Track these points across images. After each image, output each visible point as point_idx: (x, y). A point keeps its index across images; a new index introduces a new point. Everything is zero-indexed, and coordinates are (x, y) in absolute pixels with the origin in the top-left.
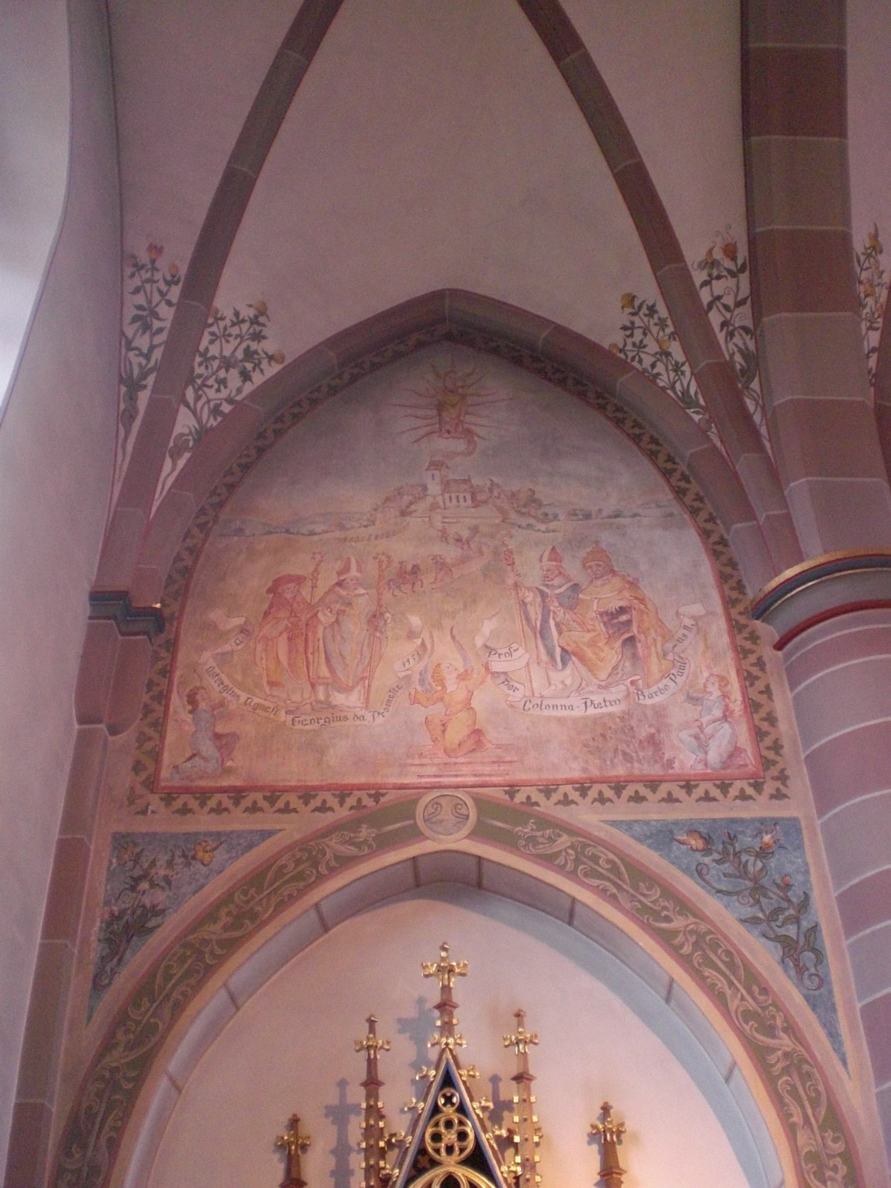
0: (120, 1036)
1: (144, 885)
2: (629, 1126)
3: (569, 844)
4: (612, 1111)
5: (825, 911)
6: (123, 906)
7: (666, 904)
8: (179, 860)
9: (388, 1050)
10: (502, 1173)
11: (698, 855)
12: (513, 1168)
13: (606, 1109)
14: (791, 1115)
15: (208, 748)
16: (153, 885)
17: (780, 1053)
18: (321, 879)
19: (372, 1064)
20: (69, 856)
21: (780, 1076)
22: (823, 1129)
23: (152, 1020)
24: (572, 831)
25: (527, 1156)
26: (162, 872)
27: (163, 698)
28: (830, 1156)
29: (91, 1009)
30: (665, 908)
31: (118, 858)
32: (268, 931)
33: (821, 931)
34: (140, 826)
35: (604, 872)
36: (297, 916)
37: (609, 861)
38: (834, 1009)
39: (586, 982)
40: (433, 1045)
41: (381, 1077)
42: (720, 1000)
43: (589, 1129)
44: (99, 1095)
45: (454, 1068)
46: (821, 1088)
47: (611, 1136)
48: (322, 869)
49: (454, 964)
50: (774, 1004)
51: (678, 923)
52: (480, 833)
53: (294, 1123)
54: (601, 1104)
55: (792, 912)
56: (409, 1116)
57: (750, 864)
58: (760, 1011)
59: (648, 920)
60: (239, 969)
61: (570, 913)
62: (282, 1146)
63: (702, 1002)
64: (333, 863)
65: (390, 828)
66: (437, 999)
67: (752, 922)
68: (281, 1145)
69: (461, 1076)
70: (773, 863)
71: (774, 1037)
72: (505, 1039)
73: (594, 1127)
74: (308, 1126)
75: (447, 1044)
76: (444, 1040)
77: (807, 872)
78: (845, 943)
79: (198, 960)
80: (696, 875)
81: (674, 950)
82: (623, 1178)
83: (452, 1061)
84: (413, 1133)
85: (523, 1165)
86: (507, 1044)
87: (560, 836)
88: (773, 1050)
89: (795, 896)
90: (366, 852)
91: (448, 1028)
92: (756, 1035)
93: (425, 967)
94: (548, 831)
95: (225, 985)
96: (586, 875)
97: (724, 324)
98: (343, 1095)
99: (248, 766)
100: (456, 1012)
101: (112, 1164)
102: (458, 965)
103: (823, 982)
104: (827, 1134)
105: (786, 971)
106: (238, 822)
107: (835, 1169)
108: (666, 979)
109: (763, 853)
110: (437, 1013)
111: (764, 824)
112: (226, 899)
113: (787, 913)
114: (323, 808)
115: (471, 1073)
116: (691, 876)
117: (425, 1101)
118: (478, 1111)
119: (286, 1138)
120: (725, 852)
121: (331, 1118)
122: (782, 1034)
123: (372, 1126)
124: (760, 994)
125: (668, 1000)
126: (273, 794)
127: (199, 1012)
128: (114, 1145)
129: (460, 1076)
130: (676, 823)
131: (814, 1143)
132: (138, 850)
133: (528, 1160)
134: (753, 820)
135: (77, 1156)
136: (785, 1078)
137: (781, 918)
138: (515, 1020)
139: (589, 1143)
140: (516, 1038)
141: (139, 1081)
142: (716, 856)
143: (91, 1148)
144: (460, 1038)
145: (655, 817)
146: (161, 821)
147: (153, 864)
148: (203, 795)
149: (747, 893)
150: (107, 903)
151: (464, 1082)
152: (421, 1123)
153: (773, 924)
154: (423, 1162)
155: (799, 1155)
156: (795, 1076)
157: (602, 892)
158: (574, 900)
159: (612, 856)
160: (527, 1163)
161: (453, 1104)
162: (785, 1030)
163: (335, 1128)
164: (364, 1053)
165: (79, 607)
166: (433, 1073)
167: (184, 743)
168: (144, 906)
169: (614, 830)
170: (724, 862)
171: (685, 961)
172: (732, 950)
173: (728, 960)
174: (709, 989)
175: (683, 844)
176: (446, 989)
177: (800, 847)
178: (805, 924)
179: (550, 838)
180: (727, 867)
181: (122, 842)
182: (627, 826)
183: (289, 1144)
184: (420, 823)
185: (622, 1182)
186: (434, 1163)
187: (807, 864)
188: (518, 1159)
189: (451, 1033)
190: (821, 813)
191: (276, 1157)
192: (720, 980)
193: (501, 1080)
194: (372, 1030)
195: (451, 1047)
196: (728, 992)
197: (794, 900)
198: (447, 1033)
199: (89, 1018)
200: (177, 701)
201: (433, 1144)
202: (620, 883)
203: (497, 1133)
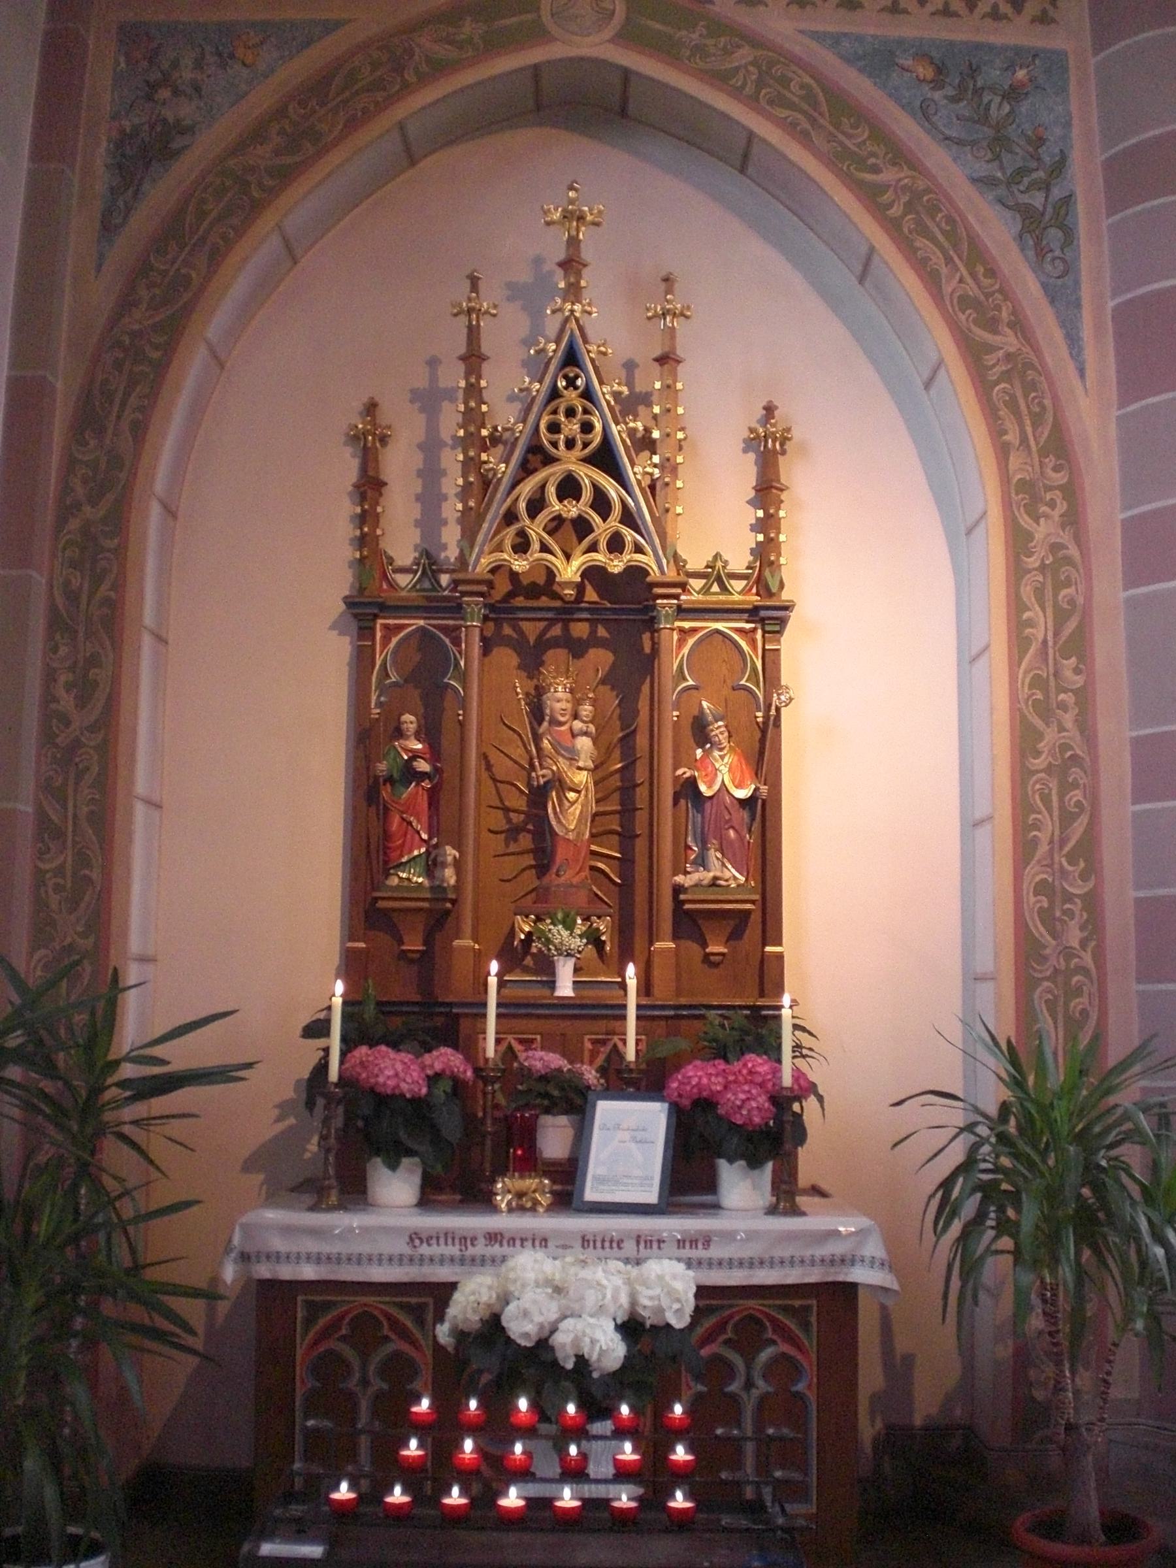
0: (143, 293)
1: (164, 94)
2: (796, 433)
3: (750, 59)
4: (776, 413)
5: (1084, 179)
6: (136, 121)
7: (875, 149)
8: (211, 59)
9: (494, 315)
10: (635, 474)
11: (926, 88)
12: (649, 470)
13: (769, 410)
14: (1005, 432)
16: (176, 92)
17: (1001, 353)
18: (407, 89)
19: (473, 333)
21: (997, 383)
22: (1043, 453)
23: (183, 271)
24: (755, 41)
25: (667, 455)
26: (187, 75)
28: (1049, 489)
29: (102, 256)
30: (873, 155)
31: (127, 55)
32: (335, 158)
33: (1075, 203)
35: (796, 99)
36: (376, 138)
37: (802, 86)
38: (1078, 305)
39: (756, 248)
40: (554, 312)
41: (485, 348)
42: (932, 280)
43: (746, 434)
44: (118, 365)
45: (580, 341)
46: (1047, 402)
47: (774, 442)
48: (410, 76)
49: (586, 209)
50: (1001, 291)
51: (888, 175)
52: (628, 36)
53: (371, 408)
54: (764, 403)
55: (1041, 174)
56: (518, 406)
57: (993, 106)
58: (982, 298)
59: (848, 166)
60: (298, 206)
61: (743, 156)
62: (354, 437)
63: (910, 280)
64: (424, 68)
65: (507, 22)
66: (561, 255)
67: (985, 183)
68: (354, 435)
69: (589, 352)
70: (1024, 107)
71: (995, 332)
72: (648, 310)
73: (751, 430)
74: (386, 415)
75: (572, 311)
76: (568, 306)
77: (1068, 125)
78: (1106, 223)
79: (243, 192)
80: (920, 114)
81: (878, 210)
82: (784, 496)
83: (577, 333)
84: (524, 421)
85: (660, 466)
86: (650, 314)
87: (739, 47)
88: (991, 349)
89: (1048, 155)
90: (470, 54)
91: (574, 292)
92: (973, 327)
93: (546, 212)
94: (723, 39)
95: (279, 226)
96: (771, 102)
98: (434, 379)
100: (586, 272)
101: (137, 455)
102: (591, 210)
103: (1069, 269)
104: (1047, 460)
105: (1022, 250)
107: (1052, 504)
108: (864, 249)
109: (1014, 94)
110: (560, 272)
111: (1017, 57)
112: (280, 112)
113: (1034, 175)
115: (602, 349)
116: (913, 115)
117: (540, 382)
118: (607, 397)
119: (360, 426)
120: (961, 88)
121: (418, 405)
122: (1007, 330)
123: (472, 409)
124: (985, 276)
125: (861, 280)
127: (245, 260)
128: (139, 431)
129: (588, 354)
130: (900, 42)
131: (1030, 469)
132: (154, 45)
133: (668, 460)
134: (1005, 48)
135: (92, 443)
136: (1003, 385)
137: (1026, 181)
138: (663, 286)
139: (745, 451)
140: (662, 309)
141: (169, 350)
142: (950, 91)
143: (110, 431)
144: (589, 304)
145: (872, 31)
147: (175, 65)
149: (985, 144)
150: (115, 117)
151: (592, 361)
152: (535, 409)
153: (1014, 188)
154: (537, 456)
155: (1008, 482)
156: (1017, 384)
157: (790, 128)
158: (751, 136)
159: (808, 80)
160: (667, 464)
161: (576, 388)
162: (1011, 325)
163: (422, 418)
164: (463, 320)
166: (553, 346)
168: (165, 120)
169: (814, 45)
170: (960, 100)
171: (892, 227)
172: (958, 219)
173: (948, 228)
174: (921, 266)
175: (907, 71)
176: (573, 242)
177: (1063, 90)
178: (1057, 193)
179: (724, 49)
180: (963, 108)
182: (835, 41)
183: (365, 434)
184: (546, 18)
185: (782, 501)
186: (549, 460)
187: (1069, 114)
188: (656, 459)
189: (577, 299)
190: (1096, 52)
191: (348, 451)
192: (934, 253)
193: (637, 366)
194: (474, 287)
195: (577, 315)
196: (944, 271)
197: (1047, 159)
198: (572, 298)
199: (99, 269)
201: (548, 435)
202: (816, 115)
203: (631, 425)
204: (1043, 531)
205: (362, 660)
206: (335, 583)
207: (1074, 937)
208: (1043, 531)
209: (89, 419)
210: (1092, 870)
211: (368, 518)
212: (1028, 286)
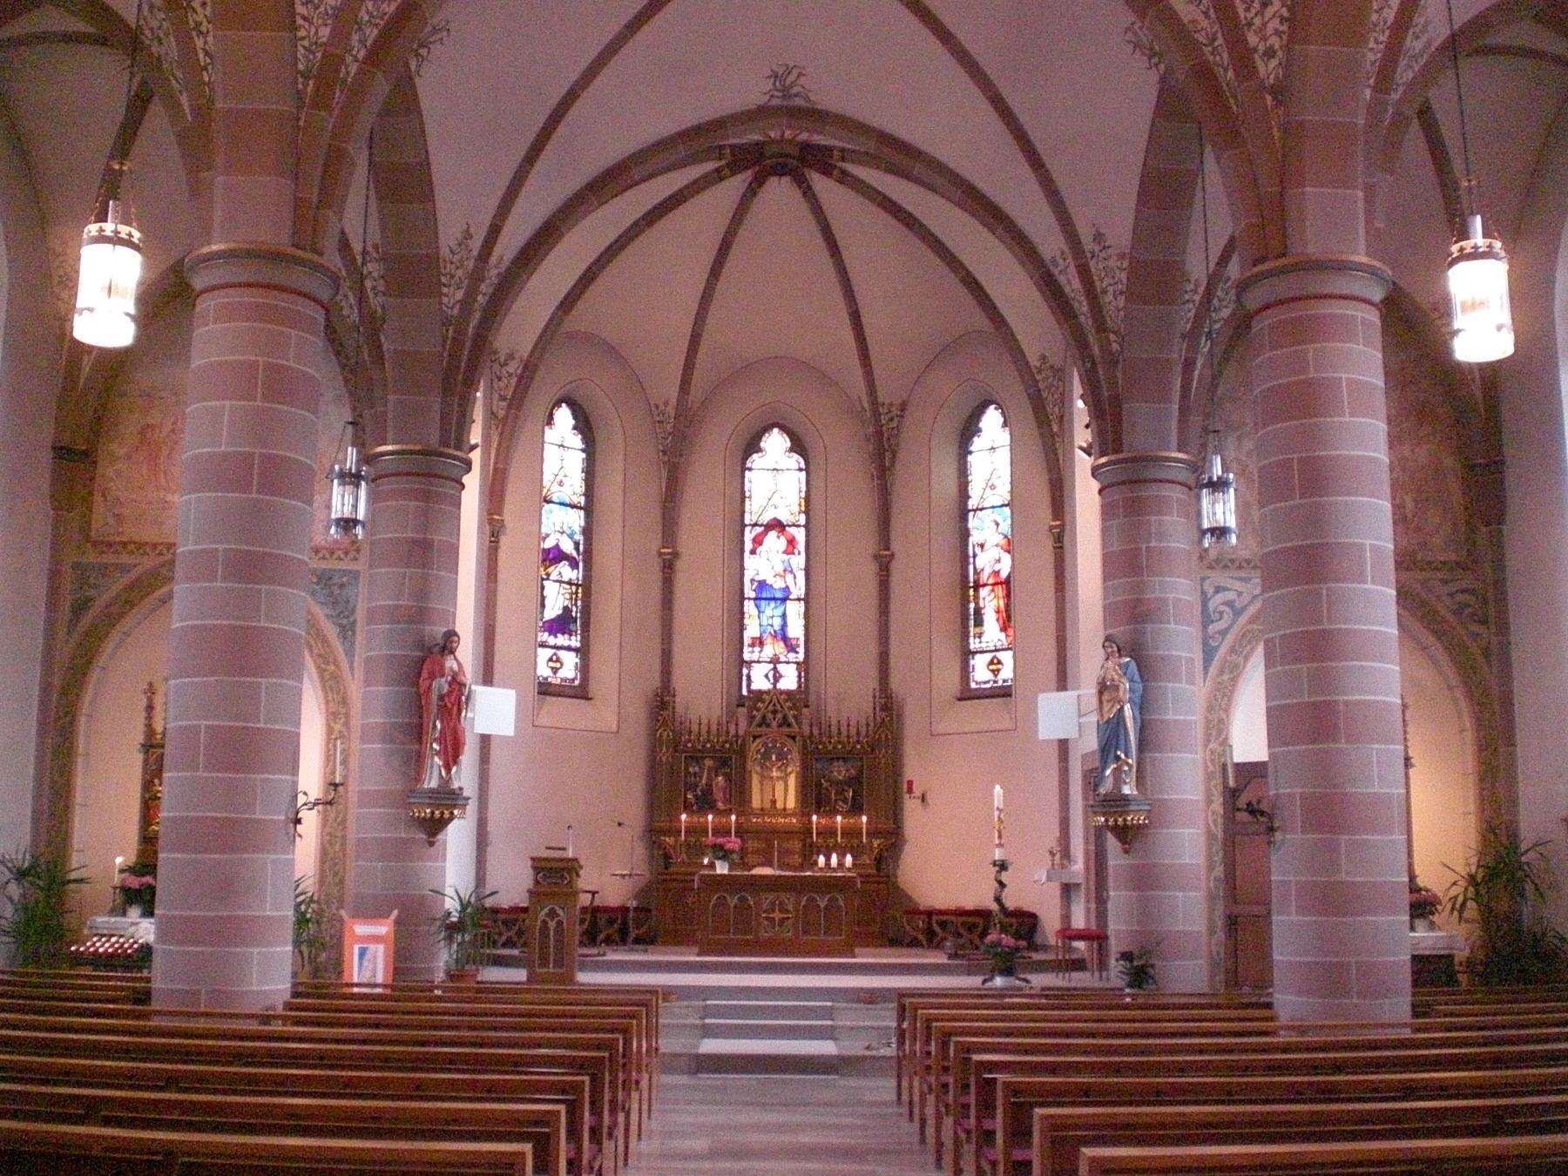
5: (360, 615)
15: (111, 521)
20: (54, 575)
27: (91, 493)
34: (84, 560)
60: (128, 622)
79: (112, 618)
97: (374, 288)
99: (132, 532)
103: (353, 644)
106: (124, 559)
109: (342, 586)
111: (345, 573)
112: (119, 595)
114: (160, 554)
126: (140, 545)
146: (91, 557)
148: (110, 545)
165: (46, 456)
167: (101, 519)
181: (76, 566)
200: (98, 498)
204: (337, 727)
205: (146, 761)
206: (140, 738)
207: (337, 848)
208: (337, 727)
209: (65, 692)
210: (345, 828)
211: (149, 718)
212: (340, 649)
